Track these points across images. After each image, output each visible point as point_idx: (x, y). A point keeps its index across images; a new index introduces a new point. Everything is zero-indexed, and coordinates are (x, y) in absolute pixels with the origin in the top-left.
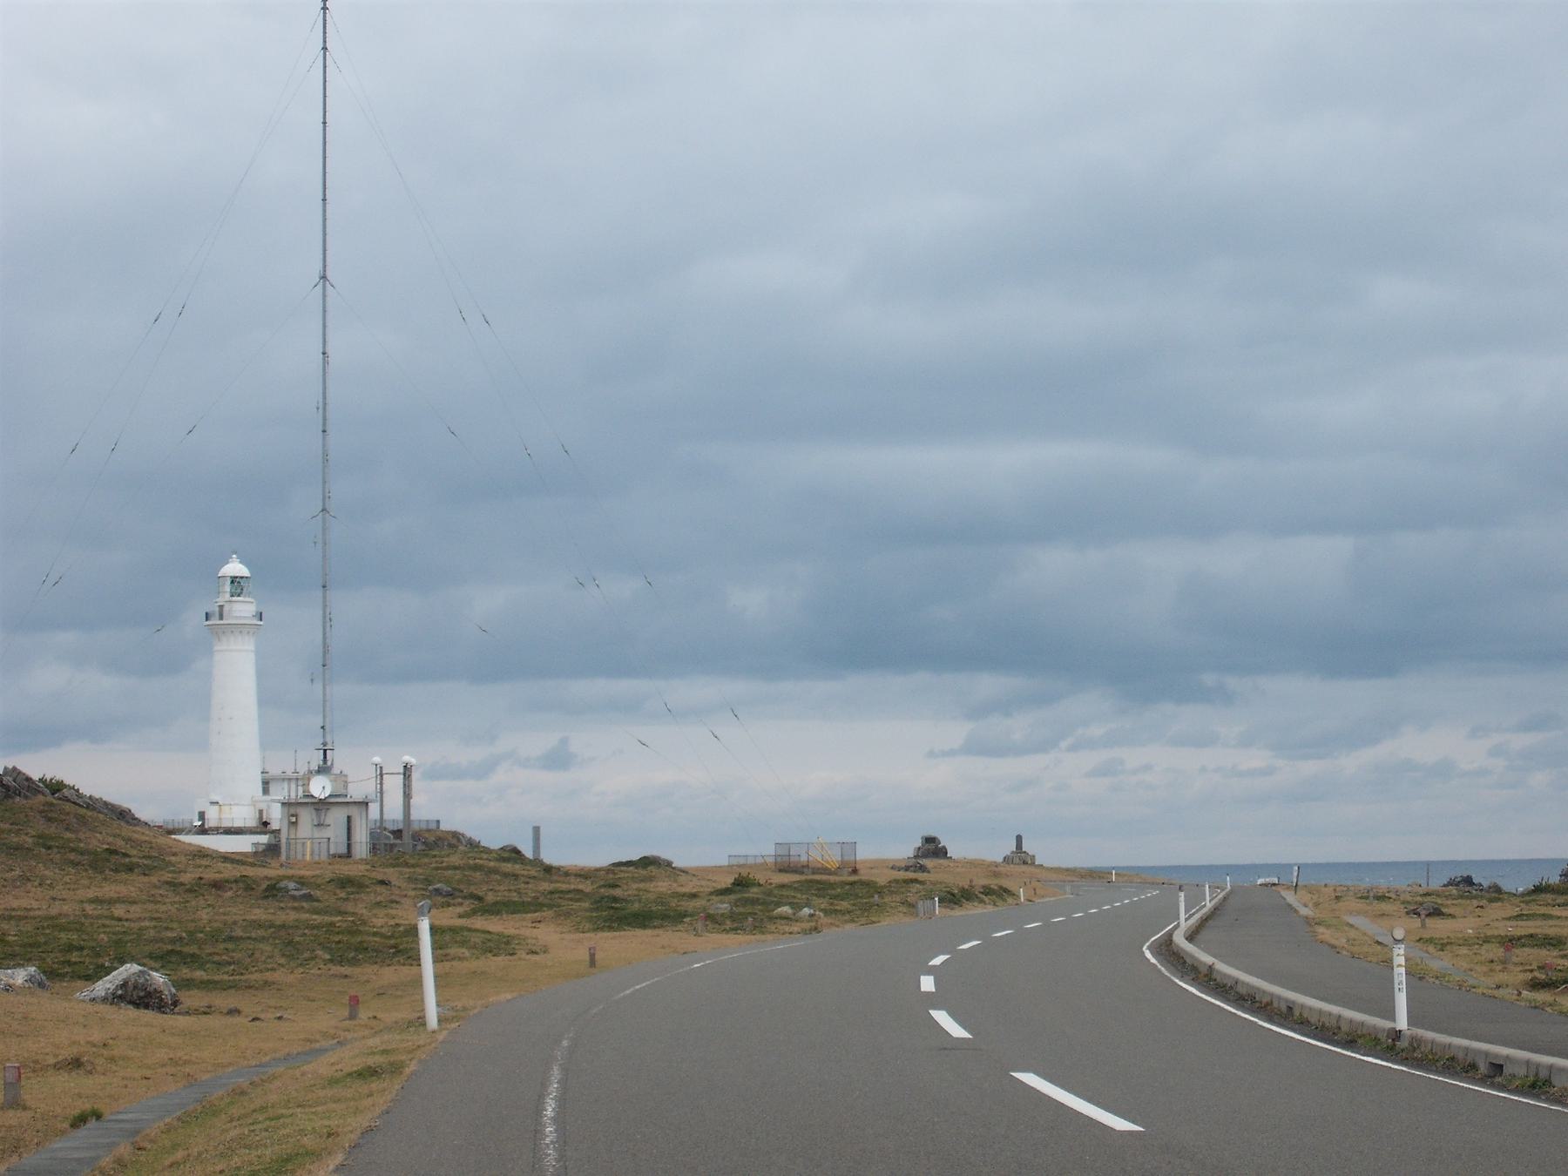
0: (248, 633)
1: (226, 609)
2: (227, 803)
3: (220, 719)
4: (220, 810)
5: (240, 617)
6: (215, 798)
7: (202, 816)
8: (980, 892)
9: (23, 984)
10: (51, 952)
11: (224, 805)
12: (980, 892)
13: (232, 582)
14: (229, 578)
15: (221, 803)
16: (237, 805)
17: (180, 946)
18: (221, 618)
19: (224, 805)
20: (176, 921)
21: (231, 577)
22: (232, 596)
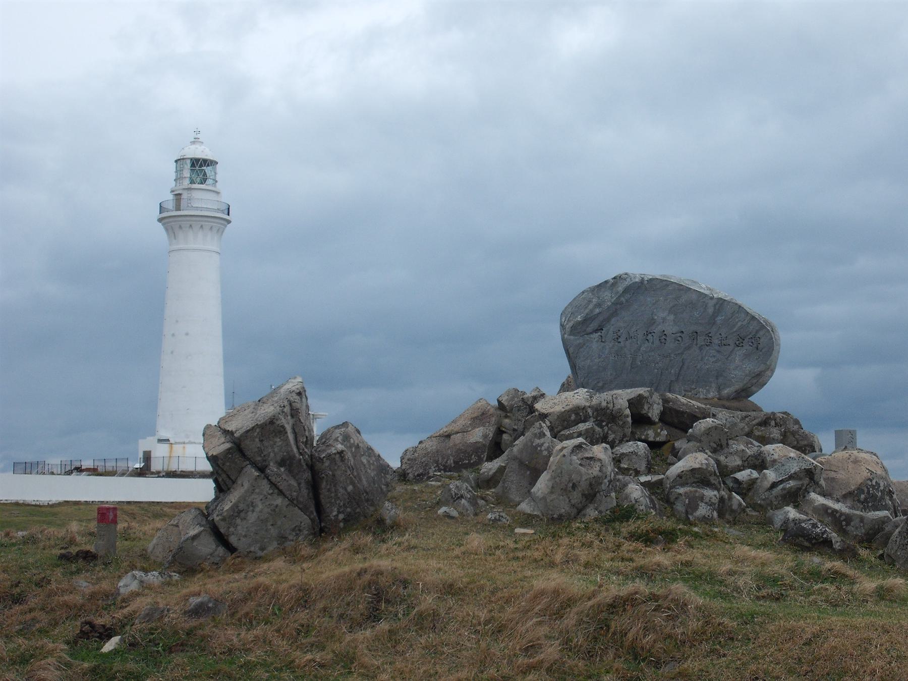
0: (211, 228)
1: (185, 195)
2: (178, 441)
3: (173, 335)
4: (171, 448)
5: (202, 209)
6: (164, 434)
7: (147, 457)
8: (201, 626)
9: (462, 679)
10: (422, 518)
11: (176, 443)
12: (201, 626)
13: (193, 165)
14: (189, 162)
15: (172, 441)
16: (190, 443)
17: (501, 553)
18: (178, 208)
19: (176, 443)
20: (568, 483)
21: (191, 159)
22: (192, 182)
